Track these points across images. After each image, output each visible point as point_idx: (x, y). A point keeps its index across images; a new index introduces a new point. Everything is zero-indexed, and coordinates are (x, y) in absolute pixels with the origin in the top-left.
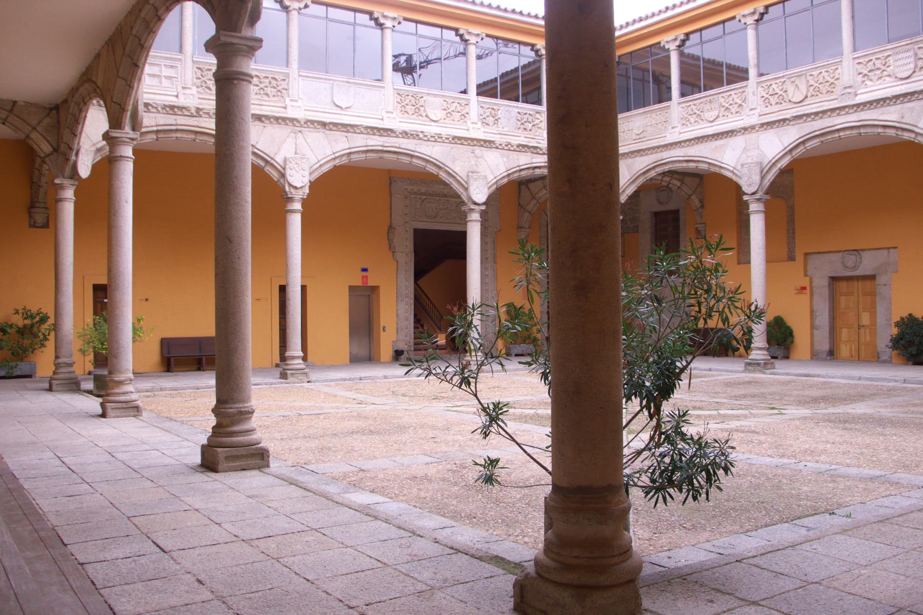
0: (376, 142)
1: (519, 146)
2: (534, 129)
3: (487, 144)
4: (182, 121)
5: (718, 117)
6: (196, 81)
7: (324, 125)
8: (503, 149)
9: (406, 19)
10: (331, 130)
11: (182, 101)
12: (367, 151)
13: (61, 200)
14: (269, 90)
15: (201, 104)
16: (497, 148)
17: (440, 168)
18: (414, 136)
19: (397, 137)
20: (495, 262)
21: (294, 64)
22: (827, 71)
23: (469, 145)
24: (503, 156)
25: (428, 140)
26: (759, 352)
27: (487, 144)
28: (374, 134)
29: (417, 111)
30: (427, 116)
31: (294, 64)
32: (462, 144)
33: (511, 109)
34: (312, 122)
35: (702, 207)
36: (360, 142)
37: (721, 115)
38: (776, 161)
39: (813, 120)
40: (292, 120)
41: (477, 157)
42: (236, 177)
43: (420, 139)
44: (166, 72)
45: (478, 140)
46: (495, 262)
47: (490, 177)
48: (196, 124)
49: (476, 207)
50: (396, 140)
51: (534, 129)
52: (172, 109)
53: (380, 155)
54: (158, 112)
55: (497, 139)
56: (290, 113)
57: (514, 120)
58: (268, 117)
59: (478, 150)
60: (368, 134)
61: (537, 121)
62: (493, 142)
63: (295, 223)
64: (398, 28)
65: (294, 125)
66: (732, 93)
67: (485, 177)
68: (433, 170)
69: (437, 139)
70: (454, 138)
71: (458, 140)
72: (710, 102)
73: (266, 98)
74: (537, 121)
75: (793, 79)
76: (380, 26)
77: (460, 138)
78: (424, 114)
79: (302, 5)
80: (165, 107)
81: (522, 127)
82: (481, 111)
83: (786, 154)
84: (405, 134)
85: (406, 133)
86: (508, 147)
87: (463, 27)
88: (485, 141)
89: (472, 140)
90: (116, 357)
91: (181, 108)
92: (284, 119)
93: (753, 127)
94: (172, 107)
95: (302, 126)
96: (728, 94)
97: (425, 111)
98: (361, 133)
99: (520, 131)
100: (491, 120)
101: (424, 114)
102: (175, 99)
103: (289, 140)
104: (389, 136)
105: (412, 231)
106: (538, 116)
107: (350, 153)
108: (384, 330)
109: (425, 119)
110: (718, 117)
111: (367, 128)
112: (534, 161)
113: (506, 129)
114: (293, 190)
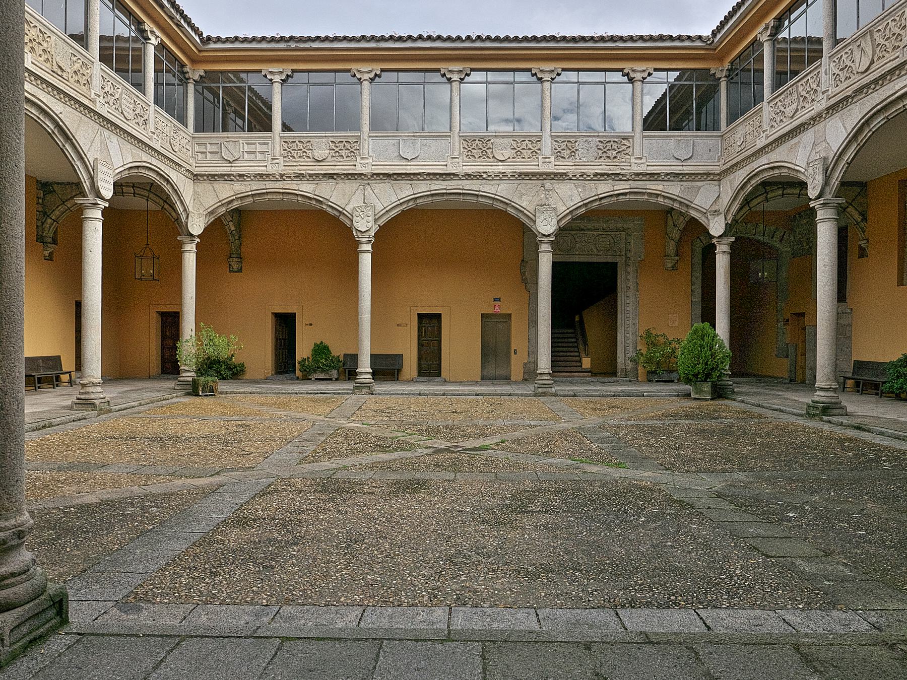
0: (438, 186)
1: (596, 174)
2: (619, 156)
4: (270, 185)
5: (797, 110)
6: (282, 152)
7: (388, 176)
8: (577, 179)
9: (655, 70)
10: (396, 180)
11: (270, 170)
12: (432, 195)
13: (184, 252)
14: (343, 153)
15: (284, 170)
16: (570, 179)
18: (478, 176)
19: (460, 179)
21: (366, 127)
22: (894, 20)
23: (538, 179)
24: (576, 187)
25: (493, 180)
26: (822, 393)
28: (437, 180)
29: (484, 154)
30: (494, 157)
31: (366, 127)
33: (590, 139)
34: (378, 175)
35: (865, 219)
36: (423, 188)
37: (799, 107)
38: (841, 153)
39: (875, 90)
40: (360, 175)
44: (259, 148)
47: (562, 209)
48: (281, 186)
49: (544, 239)
50: (460, 182)
51: (619, 156)
52: (261, 177)
53: (446, 197)
54: (252, 180)
55: (571, 170)
56: (359, 170)
57: (594, 149)
58: (338, 175)
59: (548, 184)
60: (431, 179)
61: (624, 147)
63: (366, 262)
64: (558, 79)
65: (363, 179)
66: (809, 77)
67: (554, 209)
68: (501, 206)
71: (523, 176)
72: (791, 94)
73: (340, 159)
74: (624, 147)
75: (858, 43)
76: (631, 80)
78: (491, 156)
79: (645, 75)
80: (255, 176)
81: (605, 155)
82: (556, 145)
83: (850, 141)
84: (468, 176)
85: (469, 175)
87: (627, 66)
88: (556, 174)
89: (541, 174)
91: (268, 175)
92: (353, 175)
93: (819, 115)
94: (261, 175)
95: (369, 179)
96: (805, 80)
98: (425, 180)
99: (602, 160)
100: (566, 153)
101: (491, 156)
102: (264, 168)
103: (359, 191)
104: (452, 179)
106: (624, 142)
107: (416, 198)
108: (515, 353)
109: (492, 160)
110: (797, 110)
111: (429, 174)
113: (584, 159)
114: (359, 234)
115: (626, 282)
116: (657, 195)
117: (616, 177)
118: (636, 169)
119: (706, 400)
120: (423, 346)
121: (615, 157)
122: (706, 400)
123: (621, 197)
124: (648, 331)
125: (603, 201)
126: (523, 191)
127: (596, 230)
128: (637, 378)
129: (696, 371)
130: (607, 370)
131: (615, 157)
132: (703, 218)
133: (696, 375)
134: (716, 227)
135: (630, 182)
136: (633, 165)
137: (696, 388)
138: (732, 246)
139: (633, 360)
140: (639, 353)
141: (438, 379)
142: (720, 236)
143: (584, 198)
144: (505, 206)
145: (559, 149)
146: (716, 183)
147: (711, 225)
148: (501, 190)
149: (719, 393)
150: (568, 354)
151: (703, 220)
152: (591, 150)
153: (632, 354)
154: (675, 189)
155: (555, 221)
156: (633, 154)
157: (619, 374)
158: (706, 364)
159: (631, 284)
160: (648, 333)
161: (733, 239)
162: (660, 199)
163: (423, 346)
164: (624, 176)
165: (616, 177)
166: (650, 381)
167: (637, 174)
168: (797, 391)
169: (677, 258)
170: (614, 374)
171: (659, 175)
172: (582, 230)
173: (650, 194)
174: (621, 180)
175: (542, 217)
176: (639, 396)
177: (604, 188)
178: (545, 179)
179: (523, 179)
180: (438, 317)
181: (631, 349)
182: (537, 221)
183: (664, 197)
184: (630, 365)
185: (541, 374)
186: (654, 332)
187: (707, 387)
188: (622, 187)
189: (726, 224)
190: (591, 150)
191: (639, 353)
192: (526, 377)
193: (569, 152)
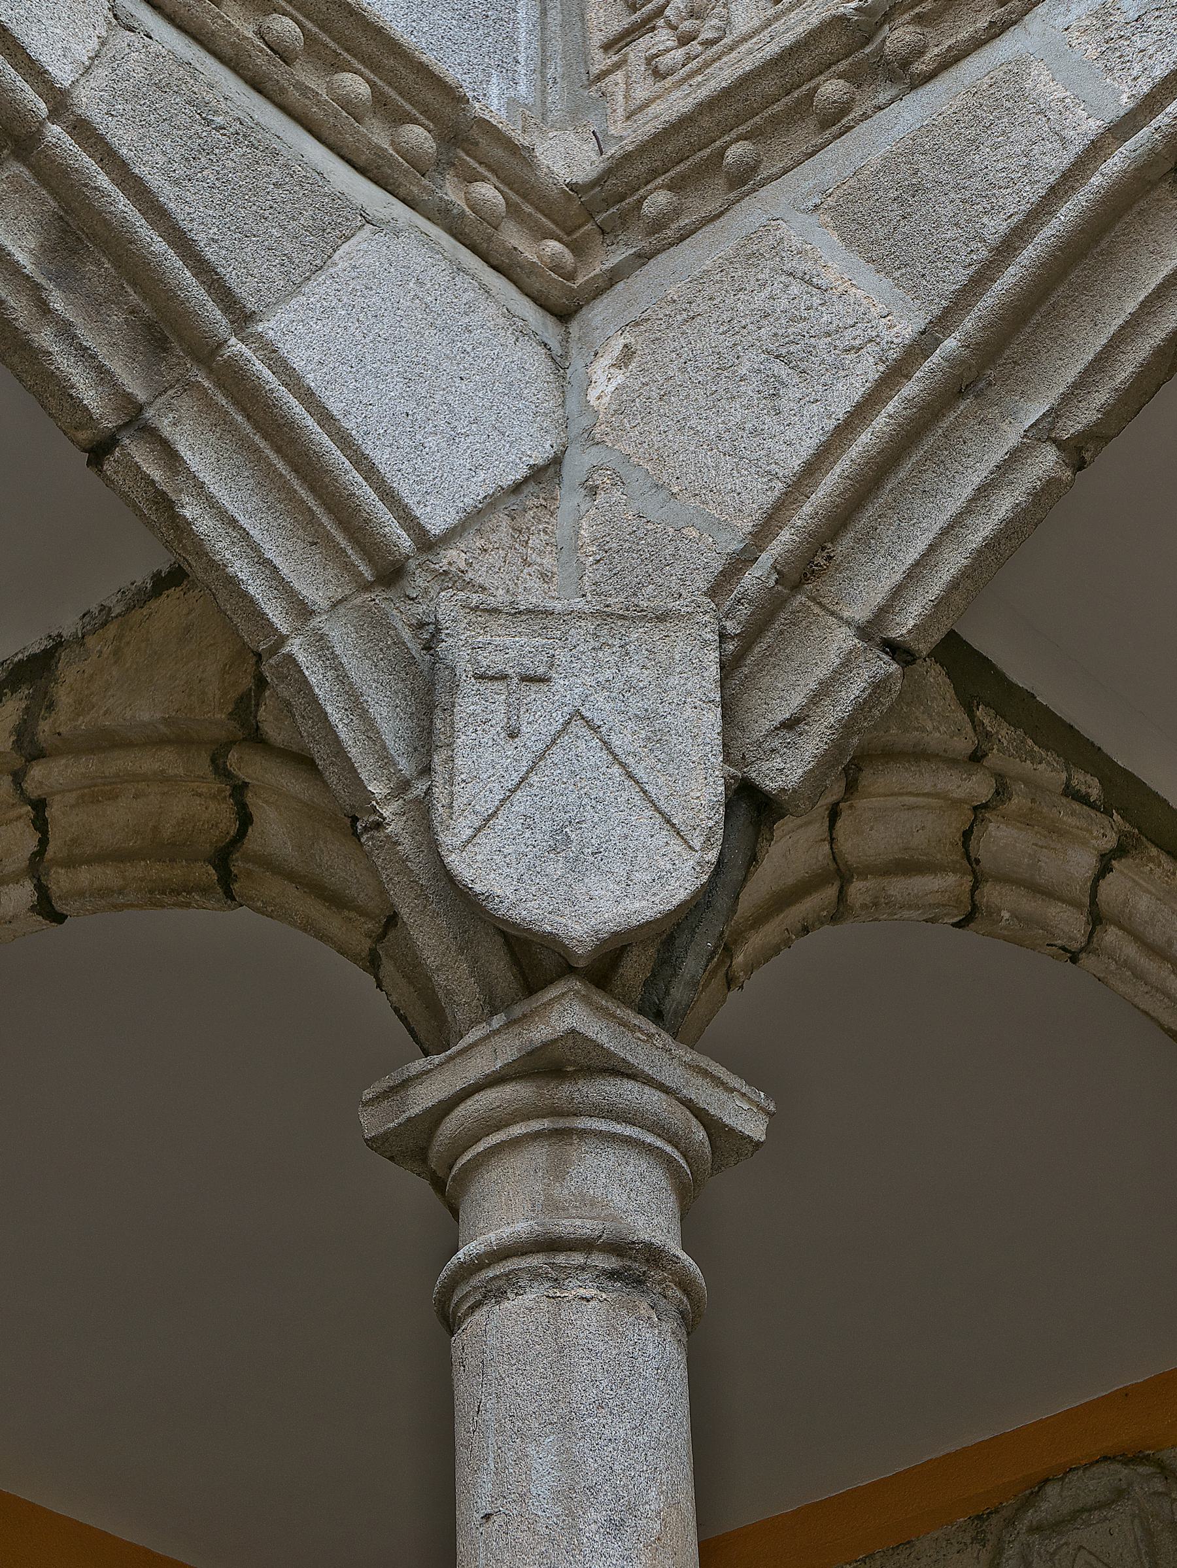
134: (579, 801)
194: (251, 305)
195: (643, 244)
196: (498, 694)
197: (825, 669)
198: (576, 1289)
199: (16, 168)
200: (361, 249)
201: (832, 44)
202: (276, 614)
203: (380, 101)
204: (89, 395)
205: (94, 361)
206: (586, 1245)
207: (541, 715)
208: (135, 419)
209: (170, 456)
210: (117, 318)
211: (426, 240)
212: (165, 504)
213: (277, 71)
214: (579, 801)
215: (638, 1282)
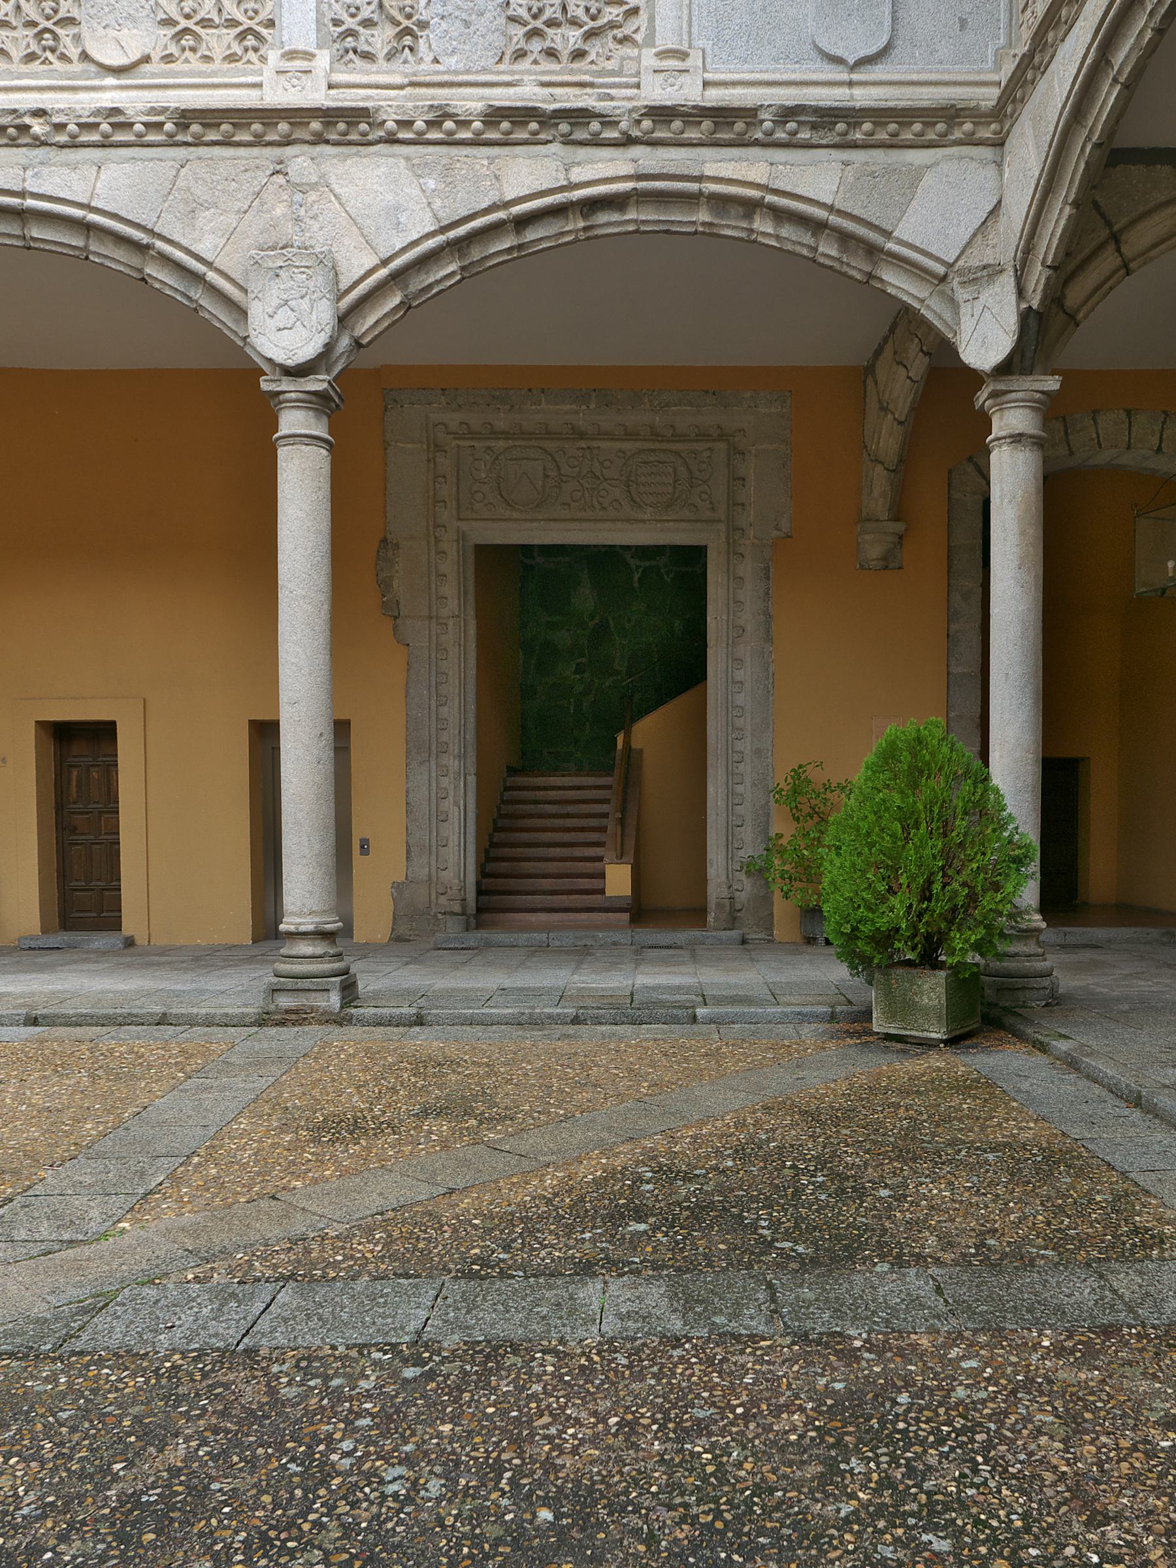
1: (494, 116)
2: (594, 49)
3: (342, 126)
16: (391, 140)
17: (141, 249)
20: (769, 639)
23: (258, 142)
24: (418, 170)
25: (74, 145)
27: (342, 126)
30: (85, 56)
32: (226, 143)
41: (302, 188)
42: (1036, 479)
43: (39, 143)
45: (297, 116)
46: (769, 639)
47: (358, 263)
55: (391, 106)
59: (301, 162)
62: (362, 113)
69: (111, 132)
70: (185, 117)
77: (210, 117)
81: (536, 45)
86: (441, 130)
88: (329, 116)
90: (811, 962)
97: (77, 38)
99: (525, 64)
100: (380, 39)
101: (73, 52)
105: (703, 543)
109: (77, 67)
112: (577, 175)
113: (451, 62)
115: (731, 609)
116: (750, 207)
117: (573, 125)
118: (657, 93)
119: (928, 1045)
120: (74, 830)
121: (579, 55)
122: (928, 1045)
123: (603, 217)
124: (797, 773)
125: (530, 235)
126: (199, 191)
127: (631, 435)
128: (770, 928)
129: (882, 923)
130: (666, 908)
131: (579, 55)
132: (936, 303)
133: (884, 940)
134: (985, 334)
135: (637, 151)
136: (646, 79)
137: (888, 994)
138: (1051, 410)
139: (758, 871)
140: (772, 846)
141: (100, 941)
142: (1005, 369)
143: (447, 218)
144: (135, 260)
145: (350, 23)
146: (987, 152)
147: (967, 324)
148: (111, 186)
149: (988, 1011)
150: (578, 852)
151: (933, 310)
152: (481, 24)
153: (751, 848)
154: (817, 178)
155: (324, 314)
156: (650, 41)
157: (710, 918)
158: (926, 894)
159: (748, 617)
160: (799, 784)
161: (1052, 384)
162: (763, 225)
163: (74, 830)
164: (608, 122)
165: (573, 125)
166: (810, 941)
167: (661, 114)
168: (1023, 533)
169: (900, 527)
170: (696, 914)
171: (750, 114)
172: (582, 436)
173: (721, 202)
174: (596, 142)
175: (275, 292)
176: (675, 1020)
177: (528, 174)
178: (287, 142)
179: (198, 143)
180: (104, 732)
181: (747, 834)
182: (256, 310)
183: (780, 215)
184: (746, 888)
185: (291, 935)
186: (813, 773)
187: (931, 990)
188: (602, 169)
189: (1025, 317)
190: (481, 24)
191: (772, 846)
192: (402, 930)
193: (391, 31)
194: (890, 229)
195: (1051, 50)
196: (969, 305)
197: (1037, 277)
198: (1005, 448)
199: (827, 231)
200: (928, 179)
201: (1026, 61)
202: (916, 305)
203: (925, 124)
204: (858, 276)
205: (857, 266)
206: (1004, 438)
207: (978, 306)
208: (870, 276)
209: (881, 280)
210: (860, 252)
211: (950, 158)
212: (884, 291)
213: (895, 141)
214: (985, 334)
215: (1020, 441)
